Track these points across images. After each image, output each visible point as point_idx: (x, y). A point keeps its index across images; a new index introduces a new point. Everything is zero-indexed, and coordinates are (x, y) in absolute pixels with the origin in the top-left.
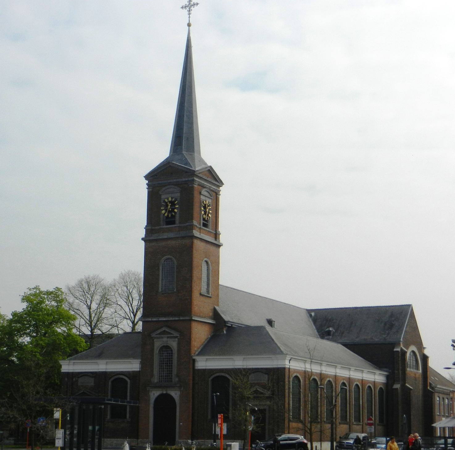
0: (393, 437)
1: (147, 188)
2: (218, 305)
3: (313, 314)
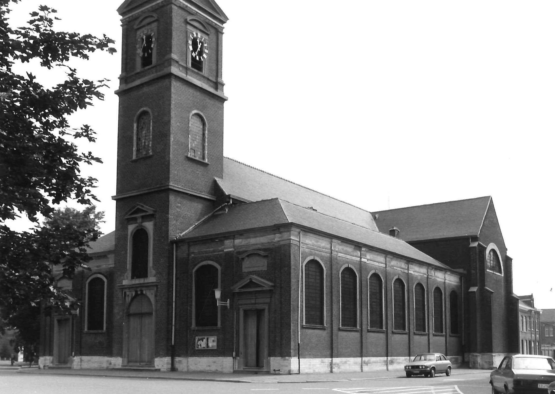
0: (56, 305)
1: (121, 26)
2: (222, 177)
3: (377, 216)
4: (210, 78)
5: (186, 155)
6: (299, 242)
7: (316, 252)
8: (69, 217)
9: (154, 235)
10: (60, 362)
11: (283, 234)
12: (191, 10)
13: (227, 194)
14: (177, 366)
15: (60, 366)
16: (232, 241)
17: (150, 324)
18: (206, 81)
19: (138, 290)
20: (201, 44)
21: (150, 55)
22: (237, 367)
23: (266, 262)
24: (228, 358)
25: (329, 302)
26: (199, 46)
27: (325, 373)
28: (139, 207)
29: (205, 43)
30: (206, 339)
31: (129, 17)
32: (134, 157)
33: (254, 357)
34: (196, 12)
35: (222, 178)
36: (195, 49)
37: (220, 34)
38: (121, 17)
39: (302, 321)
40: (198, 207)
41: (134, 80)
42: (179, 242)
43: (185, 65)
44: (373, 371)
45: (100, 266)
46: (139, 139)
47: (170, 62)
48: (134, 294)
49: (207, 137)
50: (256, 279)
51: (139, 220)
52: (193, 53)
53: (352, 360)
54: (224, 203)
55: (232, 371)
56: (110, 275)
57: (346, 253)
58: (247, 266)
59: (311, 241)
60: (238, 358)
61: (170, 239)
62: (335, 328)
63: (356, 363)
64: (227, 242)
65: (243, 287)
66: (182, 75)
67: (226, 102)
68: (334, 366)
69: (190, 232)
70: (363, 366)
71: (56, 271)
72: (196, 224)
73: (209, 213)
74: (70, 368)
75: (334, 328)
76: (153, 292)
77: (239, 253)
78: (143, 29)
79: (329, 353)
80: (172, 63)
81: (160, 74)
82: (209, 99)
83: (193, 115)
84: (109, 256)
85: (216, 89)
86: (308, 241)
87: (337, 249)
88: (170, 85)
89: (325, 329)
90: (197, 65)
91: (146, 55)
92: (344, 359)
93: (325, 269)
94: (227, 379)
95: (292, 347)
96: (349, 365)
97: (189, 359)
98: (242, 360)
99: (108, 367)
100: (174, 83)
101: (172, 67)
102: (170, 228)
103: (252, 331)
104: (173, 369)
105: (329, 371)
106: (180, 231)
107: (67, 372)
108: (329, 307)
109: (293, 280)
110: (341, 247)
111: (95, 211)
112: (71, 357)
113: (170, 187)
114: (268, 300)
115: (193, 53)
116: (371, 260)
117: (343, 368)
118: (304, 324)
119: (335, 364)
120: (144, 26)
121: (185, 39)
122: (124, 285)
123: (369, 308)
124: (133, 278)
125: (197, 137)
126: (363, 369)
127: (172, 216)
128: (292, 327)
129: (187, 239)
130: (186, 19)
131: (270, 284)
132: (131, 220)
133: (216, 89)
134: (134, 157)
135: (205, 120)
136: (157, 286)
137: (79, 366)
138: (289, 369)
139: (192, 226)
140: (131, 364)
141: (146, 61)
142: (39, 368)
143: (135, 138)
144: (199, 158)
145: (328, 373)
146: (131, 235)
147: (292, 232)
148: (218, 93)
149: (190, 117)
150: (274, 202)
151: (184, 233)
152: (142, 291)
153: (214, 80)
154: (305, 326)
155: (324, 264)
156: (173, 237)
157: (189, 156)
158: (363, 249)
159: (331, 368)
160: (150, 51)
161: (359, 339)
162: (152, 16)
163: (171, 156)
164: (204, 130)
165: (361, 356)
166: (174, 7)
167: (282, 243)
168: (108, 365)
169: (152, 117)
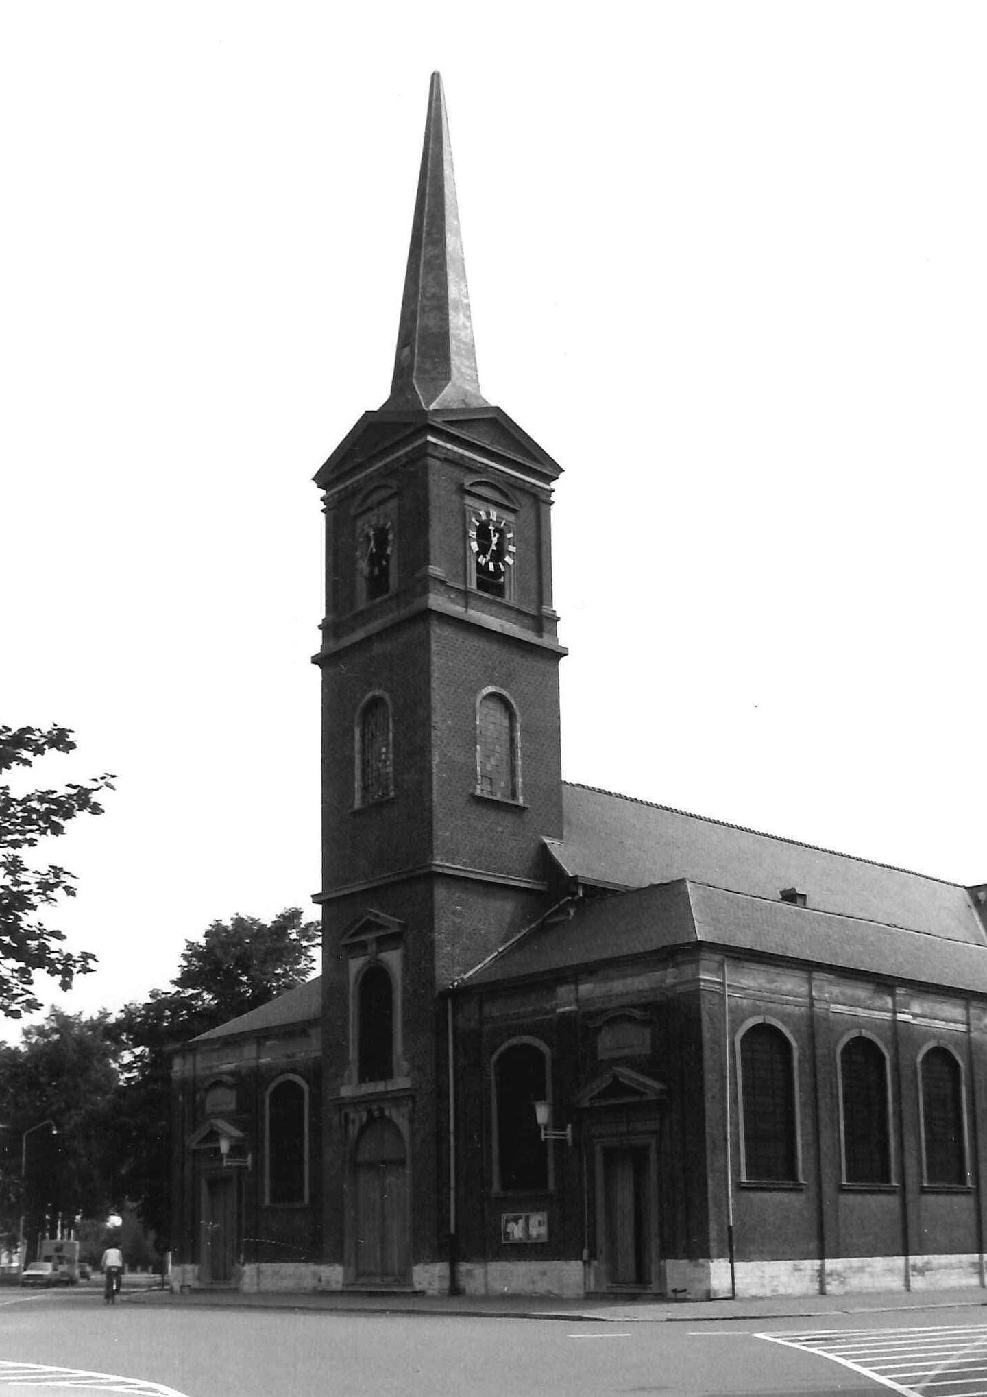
4: (524, 608)
5: (471, 791)
6: (722, 984)
7: (771, 1005)
8: (241, 939)
9: (403, 979)
10: (216, 1277)
11: (683, 967)
12: (472, 463)
13: (570, 875)
14: (463, 1282)
15: (215, 1286)
16: (573, 987)
17: (399, 1184)
18: (513, 615)
19: (374, 1107)
20: (497, 535)
21: (385, 572)
22: (592, 1282)
23: (648, 1036)
24: (573, 1263)
25: (808, 1122)
26: (495, 540)
27: (805, 1297)
28: (369, 917)
29: (510, 532)
30: (524, 1217)
31: (339, 492)
32: (357, 804)
33: (630, 1261)
34: (483, 466)
35: (560, 837)
36: (483, 550)
37: (544, 507)
38: (323, 493)
39: (737, 1172)
40: (506, 908)
41: (353, 630)
42: (462, 994)
43: (462, 587)
44: (941, 1289)
45: (294, 1055)
46: (365, 763)
47: (424, 584)
48: (365, 1117)
49: (519, 745)
50: (628, 1075)
51: (372, 948)
52: (482, 556)
53: (879, 1263)
54: (564, 898)
55: (581, 1292)
56: (315, 1074)
57: (856, 1003)
58: (607, 1043)
59: (754, 979)
60: (595, 1263)
61: (437, 988)
62: (828, 1188)
63: (891, 1271)
64: (563, 991)
65: (603, 1095)
66: (457, 609)
67: (563, 660)
68: (828, 1280)
69: (486, 969)
70: (911, 1278)
71: (203, 1069)
72: (500, 950)
73: (530, 921)
74: (236, 1291)
75: (825, 1186)
76: (405, 1111)
77: (589, 1016)
78: (369, 515)
79: (813, 1246)
80: (431, 584)
81: (404, 612)
82: (522, 657)
83: (485, 698)
84: (312, 1032)
85: (539, 631)
86: (745, 982)
87: (827, 995)
88: (429, 635)
89: (801, 1190)
90: (490, 583)
91: (376, 571)
92: (856, 1262)
93: (794, 1044)
94: (560, 1314)
95: (713, 1234)
96: (872, 1275)
97: (489, 1268)
98: (603, 1267)
99: (314, 1287)
100: (438, 630)
101: (432, 596)
102: (439, 963)
103: (625, 1198)
104: (455, 1290)
105: (817, 1292)
106: (463, 969)
107: (228, 1299)
108: (810, 1138)
109: (710, 1078)
110: (836, 990)
111: (301, 921)
112: (237, 1265)
113: (434, 869)
114: (654, 1125)
115: (482, 556)
116: (924, 1017)
117: (855, 1282)
118: (744, 1179)
119: (831, 1274)
120: (370, 509)
121: (461, 528)
122: (343, 1098)
123: (923, 1135)
124: (362, 1079)
125: (498, 749)
126: (911, 1283)
127: (443, 935)
128: (710, 1188)
129: (480, 985)
130: (463, 485)
131: (657, 1085)
132: (356, 949)
133: (539, 631)
134: (357, 804)
135: (515, 706)
136: (413, 1097)
137: (256, 1287)
138: (705, 1288)
139: (492, 953)
140: (361, 1281)
141: (378, 584)
142: (172, 1291)
143: (358, 761)
144: (503, 795)
145: (813, 1297)
146: (357, 978)
147: (703, 963)
148: (545, 642)
149: (478, 705)
150: (672, 892)
151: (470, 973)
152: (381, 1110)
153: (534, 612)
154: (744, 1183)
155: (791, 1032)
156: (446, 982)
157: (478, 792)
158: (900, 991)
159: (822, 1283)
160: (384, 563)
161: (898, 1209)
162: (385, 486)
163: (435, 797)
164: (512, 729)
165: (906, 1253)
166: (431, 461)
167: (680, 989)
168: (315, 1282)
169: (391, 710)
